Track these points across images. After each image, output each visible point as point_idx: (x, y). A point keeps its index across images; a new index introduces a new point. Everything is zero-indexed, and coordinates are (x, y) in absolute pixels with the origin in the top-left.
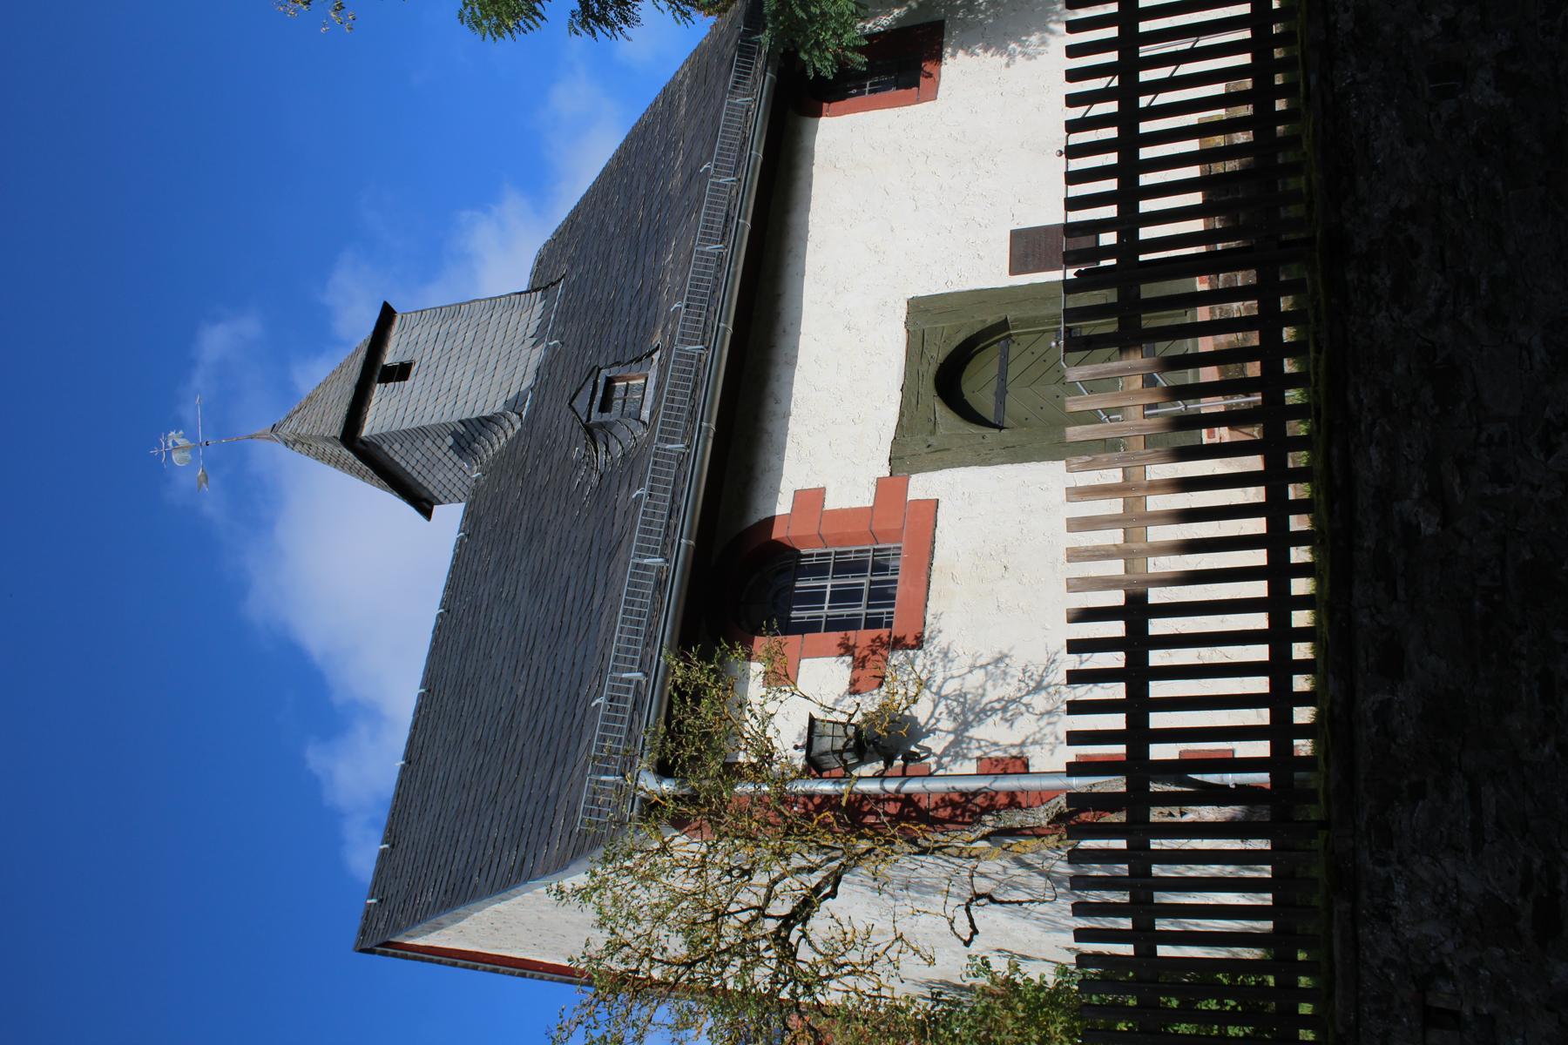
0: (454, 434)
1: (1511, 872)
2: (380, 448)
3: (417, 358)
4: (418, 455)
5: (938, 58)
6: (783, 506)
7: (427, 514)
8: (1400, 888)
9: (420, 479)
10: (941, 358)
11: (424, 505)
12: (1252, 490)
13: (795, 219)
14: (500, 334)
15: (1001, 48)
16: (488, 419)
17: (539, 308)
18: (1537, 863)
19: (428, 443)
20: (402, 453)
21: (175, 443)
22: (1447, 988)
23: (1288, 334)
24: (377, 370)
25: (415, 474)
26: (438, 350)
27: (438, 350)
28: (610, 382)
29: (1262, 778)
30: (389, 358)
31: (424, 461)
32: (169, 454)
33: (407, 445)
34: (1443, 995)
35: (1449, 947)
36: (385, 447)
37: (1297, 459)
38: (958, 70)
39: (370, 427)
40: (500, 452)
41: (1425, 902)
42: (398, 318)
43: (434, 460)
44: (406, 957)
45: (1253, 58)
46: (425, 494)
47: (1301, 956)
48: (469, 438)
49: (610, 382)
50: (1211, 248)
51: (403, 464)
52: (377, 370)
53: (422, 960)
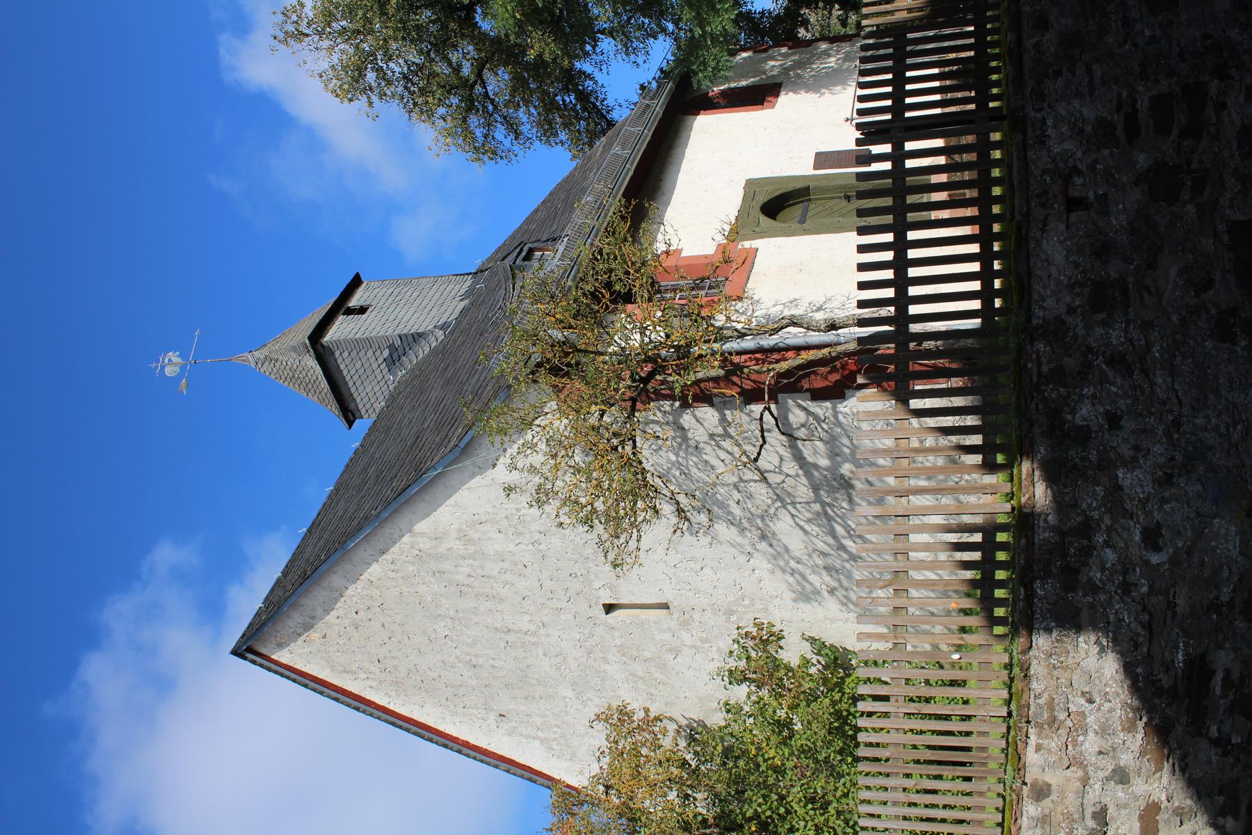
0: (392, 347)
1: (1111, 101)
2: (333, 353)
3: (374, 304)
4: (359, 365)
5: (777, 95)
6: (660, 247)
7: (350, 424)
8: (1050, 122)
9: (353, 390)
10: (766, 200)
11: (349, 415)
12: (974, 437)
13: (677, 151)
14: (438, 294)
15: (816, 92)
16: (420, 335)
17: (468, 283)
18: (1125, 94)
19: (370, 353)
20: (347, 361)
21: (170, 360)
22: (1078, 181)
23: (996, 228)
24: (340, 307)
25: (350, 384)
26: (390, 300)
27: (390, 300)
28: (531, 251)
29: (975, 323)
30: (354, 302)
31: (361, 372)
32: (163, 367)
33: (354, 354)
34: (1078, 187)
35: (1079, 154)
36: (337, 354)
37: (996, 173)
38: (786, 100)
39: (330, 336)
40: (424, 359)
41: (1064, 129)
42: (363, 286)
43: (369, 372)
44: (269, 669)
45: (981, 247)
46: (352, 406)
47: (989, 26)
48: (400, 351)
49: (531, 251)
50: (944, 96)
51: (345, 373)
52: (340, 307)
53: (282, 675)
